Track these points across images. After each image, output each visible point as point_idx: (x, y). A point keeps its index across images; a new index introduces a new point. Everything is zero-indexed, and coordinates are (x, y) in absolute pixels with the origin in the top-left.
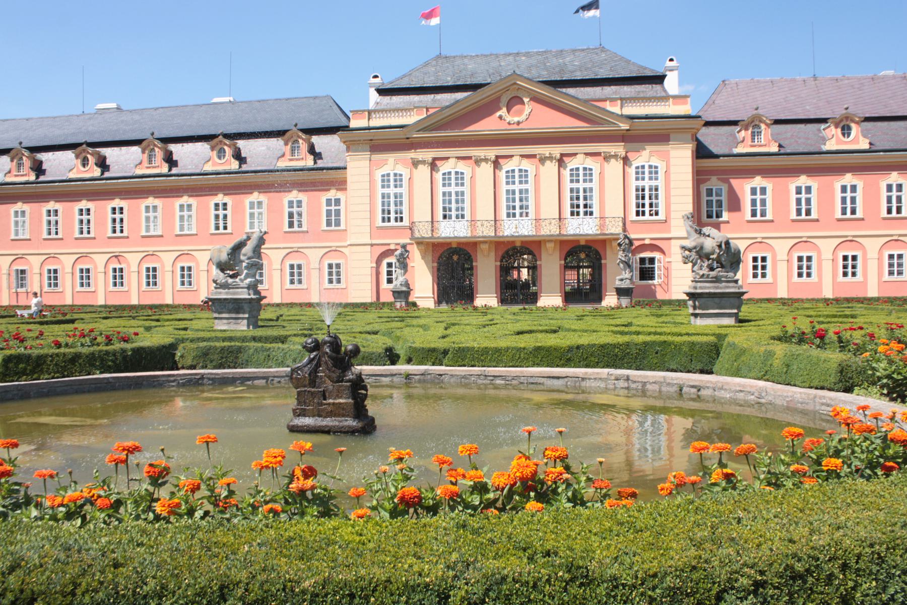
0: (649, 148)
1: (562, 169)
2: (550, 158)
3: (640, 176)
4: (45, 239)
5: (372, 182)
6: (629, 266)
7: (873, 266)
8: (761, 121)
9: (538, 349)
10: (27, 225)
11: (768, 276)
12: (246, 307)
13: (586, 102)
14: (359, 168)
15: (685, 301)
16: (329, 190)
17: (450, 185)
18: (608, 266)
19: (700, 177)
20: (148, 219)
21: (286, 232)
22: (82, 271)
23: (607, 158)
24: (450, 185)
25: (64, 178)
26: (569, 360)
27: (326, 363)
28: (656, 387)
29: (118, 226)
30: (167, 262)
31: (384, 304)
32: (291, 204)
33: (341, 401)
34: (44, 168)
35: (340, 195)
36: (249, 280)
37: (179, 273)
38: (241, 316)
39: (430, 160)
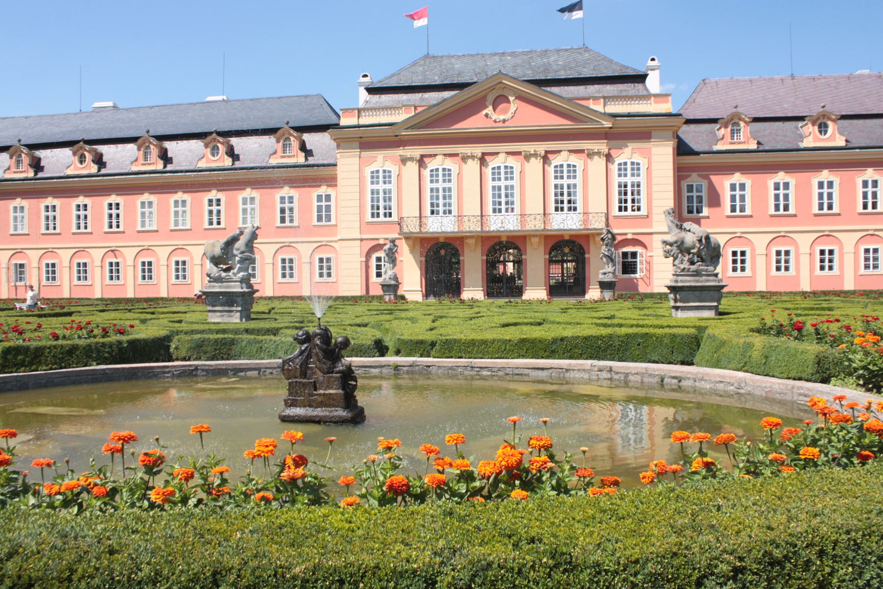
0: (631, 146)
1: (546, 166)
2: (535, 155)
3: (623, 172)
4: (43, 234)
5: (361, 178)
6: (612, 260)
7: (849, 260)
8: (740, 119)
9: (523, 341)
10: (26, 220)
11: (747, 270)
12: (239, 299)
13: (571, 99)
14: (349, 165)
15: (666, 295)
16: (319, 186)
17: (437, 181)
18: (591, 260)
19: (680, 173)
20: (143, 214)
21: (278, 227)
22: (867, 251)
23: (591, 155)
24: (437, 181)
25: (62, 175)
26: (553, 352)
27: (317, 354)
28: (638, 378)
29: (114, 221)
30: (161, 257)
31: (373, 297)
32: (282, 199)
33: (332, 391)
34: (42, 165)
35: (330, 191)
36: (242, 274)
37: (173, 267)
38: (234, 309)
39: (418, 157)
